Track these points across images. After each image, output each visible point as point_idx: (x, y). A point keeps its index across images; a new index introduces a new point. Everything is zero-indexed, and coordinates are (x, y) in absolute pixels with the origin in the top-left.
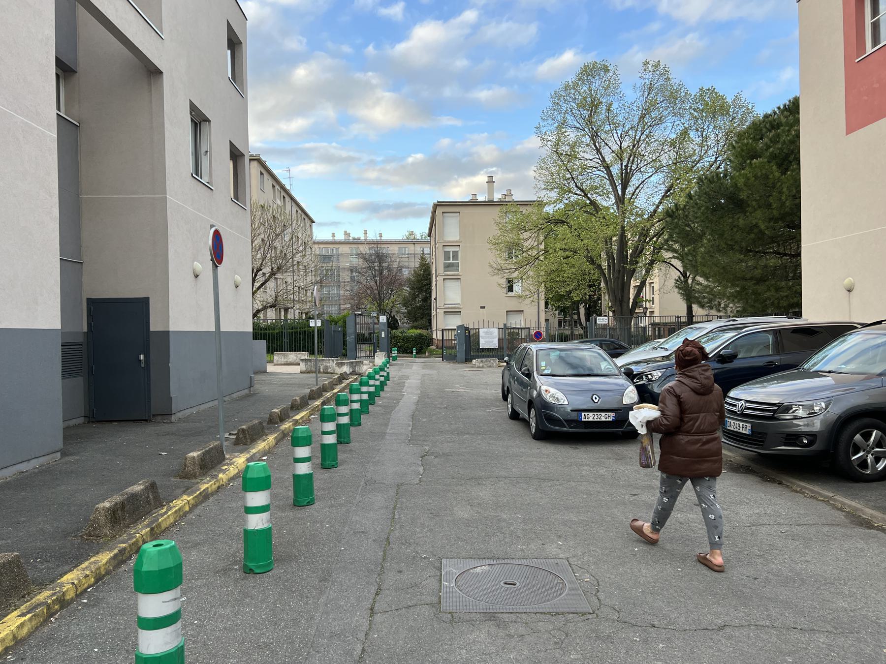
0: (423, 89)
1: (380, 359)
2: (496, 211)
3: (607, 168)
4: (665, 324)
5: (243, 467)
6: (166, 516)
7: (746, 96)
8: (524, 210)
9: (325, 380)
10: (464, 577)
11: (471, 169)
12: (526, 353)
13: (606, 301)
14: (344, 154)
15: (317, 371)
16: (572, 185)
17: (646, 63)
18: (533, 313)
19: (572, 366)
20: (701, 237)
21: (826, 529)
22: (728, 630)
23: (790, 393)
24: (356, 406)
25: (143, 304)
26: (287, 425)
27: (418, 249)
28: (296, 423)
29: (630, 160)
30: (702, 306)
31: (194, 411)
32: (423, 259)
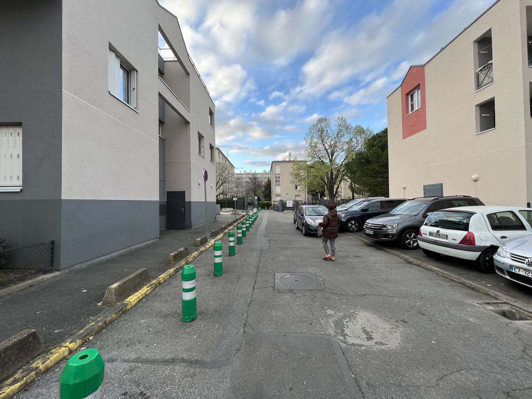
0: (270, 127)
1: (255, 210)
2: (291, 164)
3: (327, 150)
4: (345, 200)
5: (213, 243)
6: (190, 258)
7: (371, 128)
8: (300, 163)
9: (238, 217)
10: (282, 279)
11: (285, 151)
12: (301, 208)
13: (327, 192)
14: (245, 147)
15: (236, 214)
16: (316, 156)
17: (339, 118)
18: (303, 196)
19: (316, 213)
20: (357, 172)
21: (397, 265)
22: (366, 296)
23: (386, 221)
24: (248, 225)
25: (183, 193)
26: (226, 231)
27: (267, 176)
28: (229, 230)
29: (334, 147)
30: (357, 194)
31: (198, 226)
32: (268, 179)
